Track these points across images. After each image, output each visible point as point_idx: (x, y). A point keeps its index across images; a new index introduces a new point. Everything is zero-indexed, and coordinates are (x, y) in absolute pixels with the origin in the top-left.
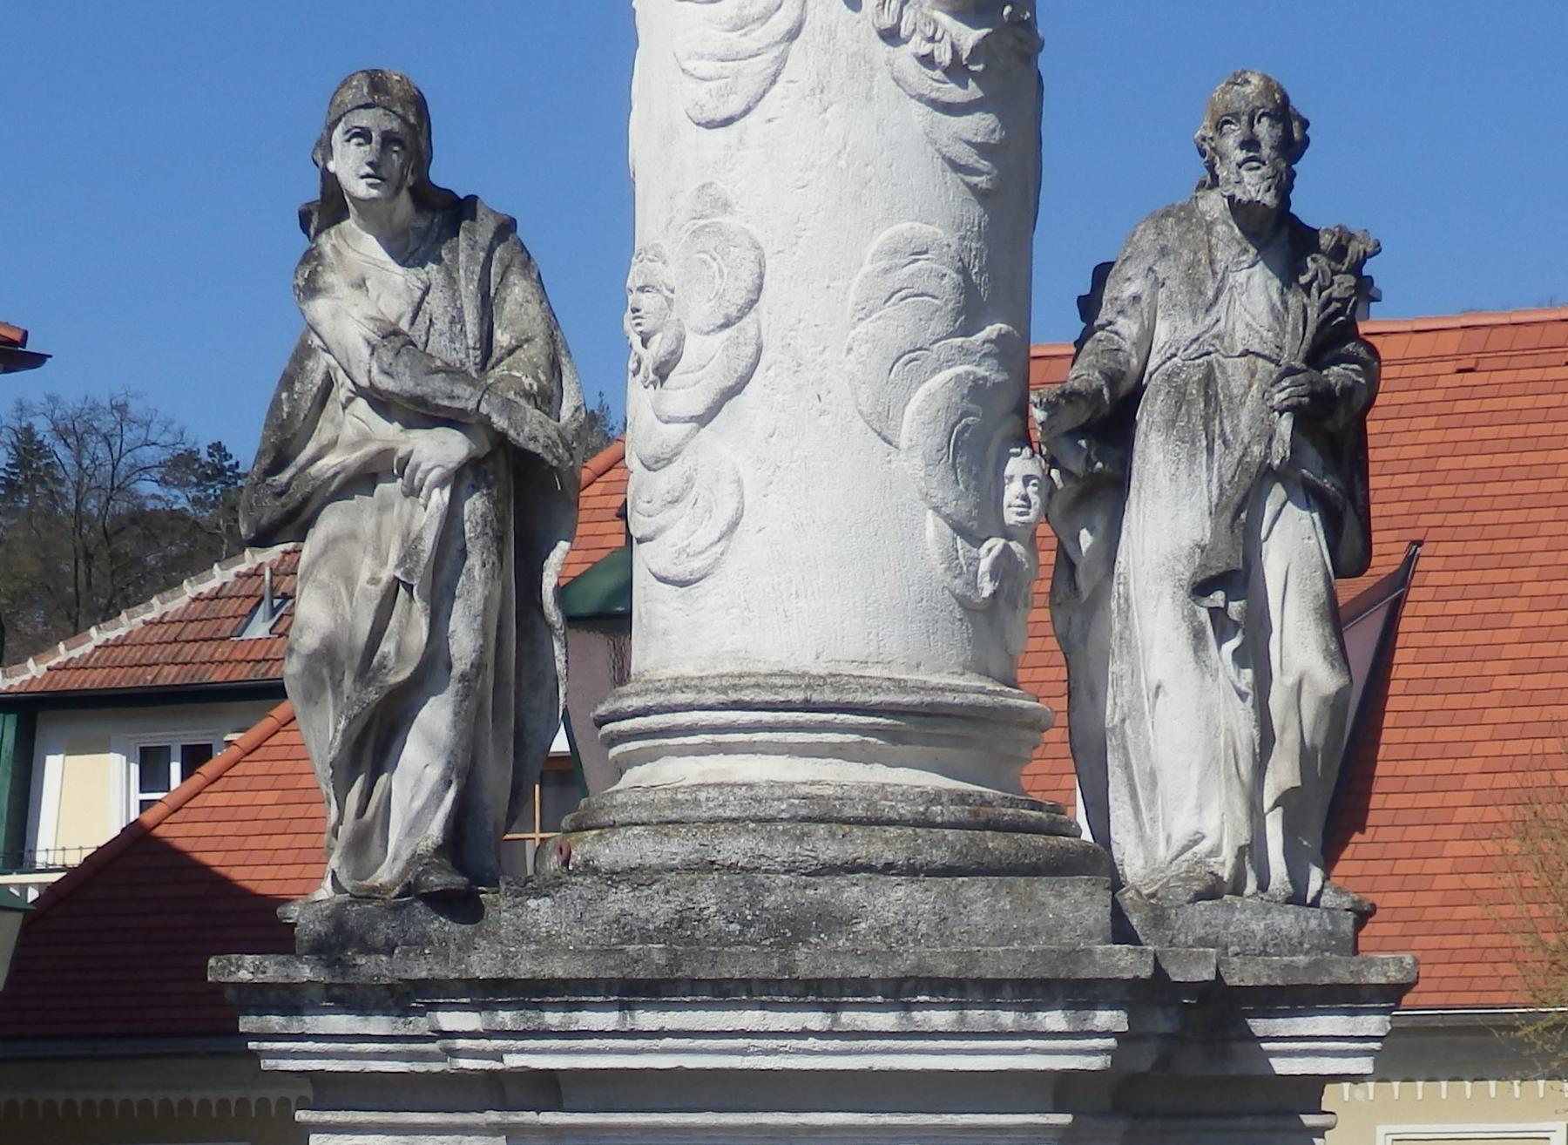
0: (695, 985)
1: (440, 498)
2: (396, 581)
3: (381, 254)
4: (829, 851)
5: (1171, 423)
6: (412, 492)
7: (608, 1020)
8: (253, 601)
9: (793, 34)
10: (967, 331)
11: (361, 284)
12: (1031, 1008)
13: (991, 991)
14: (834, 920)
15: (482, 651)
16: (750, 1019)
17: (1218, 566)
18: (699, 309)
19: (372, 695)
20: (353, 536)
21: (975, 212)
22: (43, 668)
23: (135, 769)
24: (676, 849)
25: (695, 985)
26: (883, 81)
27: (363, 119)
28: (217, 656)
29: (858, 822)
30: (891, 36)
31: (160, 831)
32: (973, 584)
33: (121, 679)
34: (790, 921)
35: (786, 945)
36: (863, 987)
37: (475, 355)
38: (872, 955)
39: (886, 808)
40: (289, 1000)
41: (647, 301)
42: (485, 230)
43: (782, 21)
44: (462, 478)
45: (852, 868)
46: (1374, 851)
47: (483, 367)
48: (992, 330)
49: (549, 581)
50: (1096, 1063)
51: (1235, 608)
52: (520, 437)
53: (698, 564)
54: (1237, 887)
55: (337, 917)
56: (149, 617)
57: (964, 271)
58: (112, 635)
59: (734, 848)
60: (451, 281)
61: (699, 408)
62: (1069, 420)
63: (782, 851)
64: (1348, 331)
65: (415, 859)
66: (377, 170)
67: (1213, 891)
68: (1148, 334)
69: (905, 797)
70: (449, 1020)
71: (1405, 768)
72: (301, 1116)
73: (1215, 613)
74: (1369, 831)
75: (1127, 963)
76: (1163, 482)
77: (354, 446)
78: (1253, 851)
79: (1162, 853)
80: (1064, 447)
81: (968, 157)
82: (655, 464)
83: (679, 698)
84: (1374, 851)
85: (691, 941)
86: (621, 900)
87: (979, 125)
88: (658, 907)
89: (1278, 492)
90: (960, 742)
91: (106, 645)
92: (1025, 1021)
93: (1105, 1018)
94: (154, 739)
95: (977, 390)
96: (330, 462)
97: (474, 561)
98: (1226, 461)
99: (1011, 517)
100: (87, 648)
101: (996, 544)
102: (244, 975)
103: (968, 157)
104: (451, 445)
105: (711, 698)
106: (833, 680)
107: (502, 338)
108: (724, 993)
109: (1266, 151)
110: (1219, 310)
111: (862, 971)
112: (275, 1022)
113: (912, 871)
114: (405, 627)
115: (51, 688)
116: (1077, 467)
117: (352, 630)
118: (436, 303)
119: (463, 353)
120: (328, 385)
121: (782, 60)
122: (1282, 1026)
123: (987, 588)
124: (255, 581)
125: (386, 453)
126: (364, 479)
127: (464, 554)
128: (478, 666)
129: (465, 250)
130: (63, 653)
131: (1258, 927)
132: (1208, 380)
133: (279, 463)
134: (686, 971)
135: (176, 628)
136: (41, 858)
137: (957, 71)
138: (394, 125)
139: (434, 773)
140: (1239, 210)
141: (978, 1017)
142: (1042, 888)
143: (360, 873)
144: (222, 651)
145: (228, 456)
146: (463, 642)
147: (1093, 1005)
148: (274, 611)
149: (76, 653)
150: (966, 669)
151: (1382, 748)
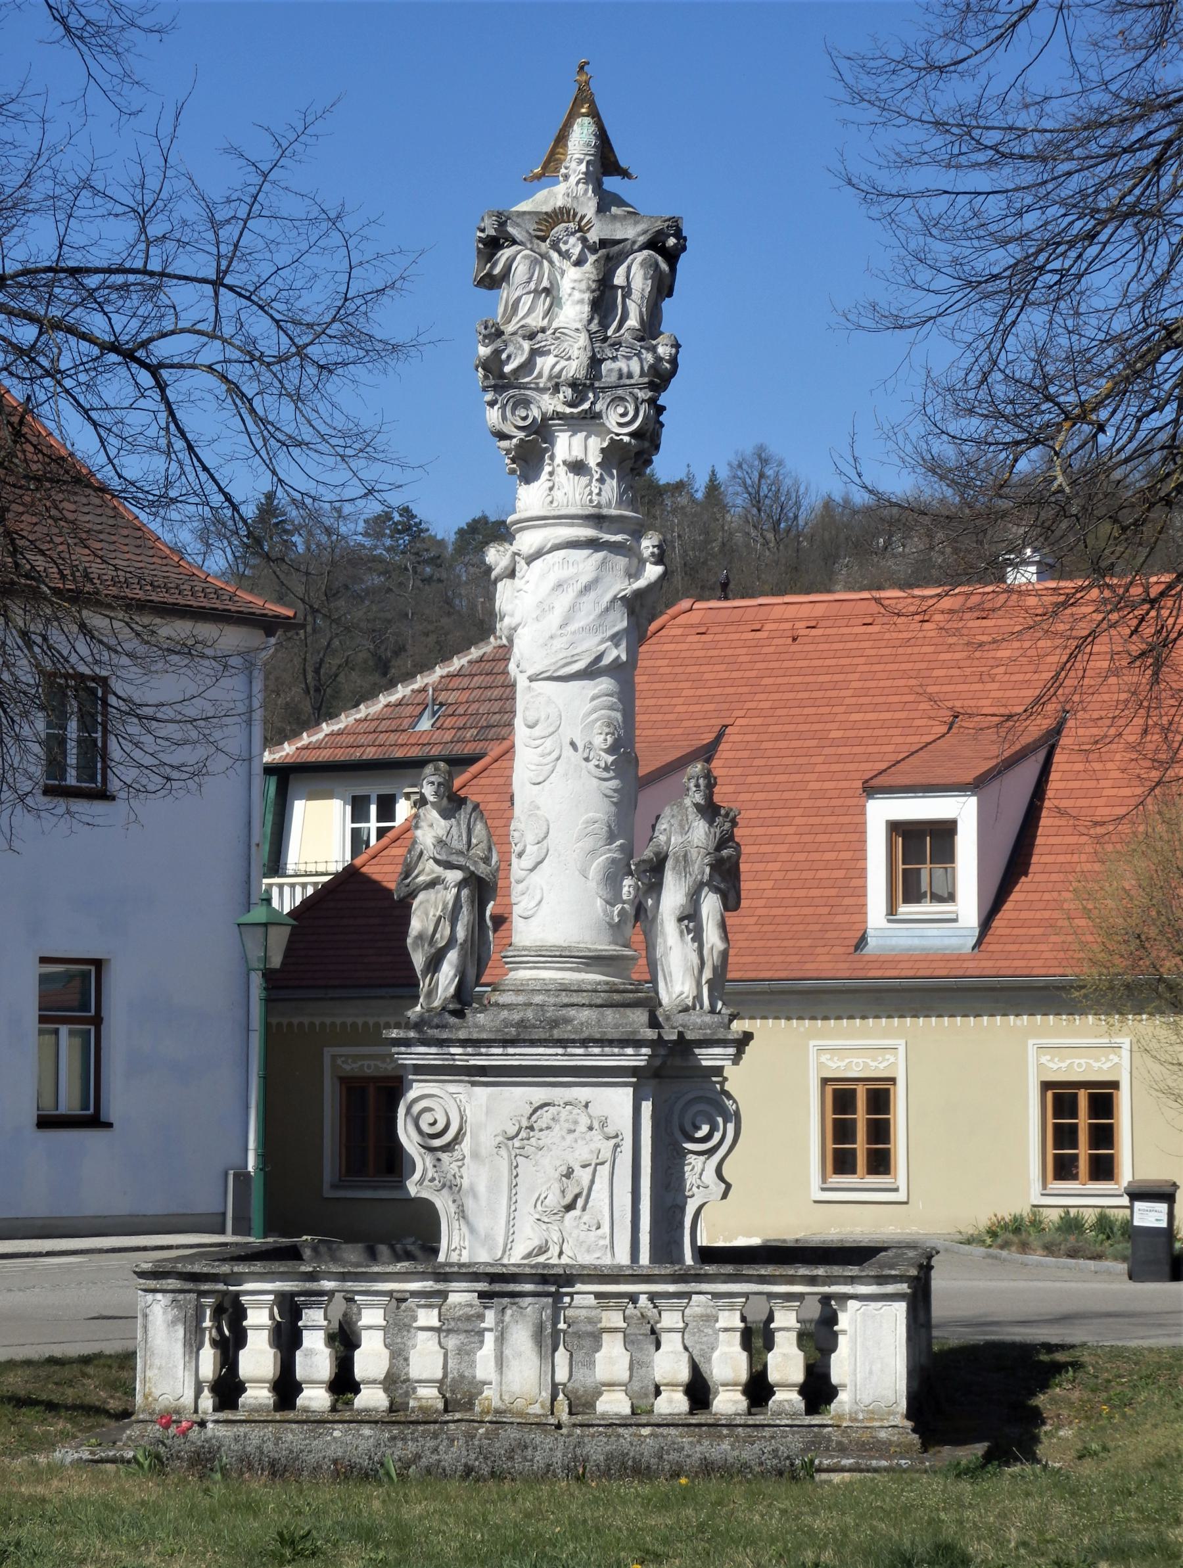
0: (524, 1041)
1: (455, 891)
2: (440, 917)
3: (437, 816)
4: (566, 1000)
5: (674, 869)
6: (446, 888)
7: (499, 1051)
8: (420, 708)
9: (558, 759)
10: (610, 844)
11: (431, 825)
12: (623, 1047)
13: (611, 1043)
14: (567, 1021)
15: (467, 936)
16: (541, 1050)
17: (686, 913)
18: (530, 838)
19: (433, 950)
20: (428, 901)
21: (613, 809)
22: (294, 748)
23: (349, 808)
24: (521, 999)
25: (524, 1041)
26: (584, 772)
27: (432, 779)
28: (400, 741)
29: (575, 991)
30: (587, 759)
31: (364, 870)
32: (612, 918)
33: (341, 755)
34: (554, 1021)
35: (552, 1028)
36: (573, 1041)
37: (466, 847)
38: (576, 1032)
39: (584, 987)
40: (407, 1043)
41: (516, 834)
42: (469, 807)
43: (555, 755)
44: (461, 885)
45: (573, 1005)
46: (1033, 887)
47: (468, 850)
48: (618, 843)
49: (488, 913)
50: (642, 1063)
51: (691, 925)
52: (478, 873)
53: (530, 913)
54: (694, 1008)
55: (421, 1016)
56: (358, 716)
57: (609, 826)
58: (336, 728)
59: (538, 999)
60: (459, 824)
61: (530, 867)
62: (642, 868)
63: (552, 1000)
64: (731, 837)
65: (445, 999)
66: (436, 793)
67: (686, 1009)
68: (669, 839)
69: (590, 983)
70: (453, 1050)
71: (1053, 840)
72: (411, 1077)
73: (687, 927)
74: (1030, 876)
75: (651, 1034)
76: (672, 886)
77: (428, 874)
78: (698, 997)
79: (674, 996)
80: (642, 876)
81: (611, 793)
82: (519, 882)
83: (524, 953)
84: (1033, 887)
85: (525, 1027)
86: (505, 1014)
87: (614, 784)
88: (516, 1016)
89: (706, 889)
90: (608, 966)
91: (332, 734)
92: (621, 1051)
93: (644, 1051)
94: (360, 791)
95: (613, 861)
96: (421, 879)
97: (464, 909)
98: (690, 880)
99: (625, 897)
100: (321, 736)
101: (619, 906)
102: (394, 1035)
103: (611, 793)
104: (454, 876)
105: (533, 953)
106: (569, 948)
107: (474, 841)
108: (533, 1043)
109: (702, 788)
110: (689, 834)
111: (573, 1037)
112: (403, 1049)
113: (590, 1006)
114: (443, 930)
115: (299, 760)
116: (646, 881)
117: (427, 929)
118: (454, 831)
119: (461, 845)
120: (421, 853)
121: (555, 766)
122: (704, 1051)
123: (617, 920)
124: (422, 696)
125: (438, 877)
126: (432, 884)
127: (461, 907)
128: (465, 941)
129: (463, 815)
130: (306, 739)
131: (699, 1021)
132: (685, 856)
133: (406, 877)
134: (522, 1037)
135: (375, 723)
136: (291, 868)
137: (606, 769)
138: (441, 780)
139: (452, 973)
140: (697, 805)
141: (607, 1050)
142: (628, 1011)
143: (429, 1004)
144: (403, 738)
145: (414, 517)
146: (461, 934)
147: (641, 1047)
148: (434, 713)
149: (314, 739)
150: (610, 943)
151: (1040, 829)
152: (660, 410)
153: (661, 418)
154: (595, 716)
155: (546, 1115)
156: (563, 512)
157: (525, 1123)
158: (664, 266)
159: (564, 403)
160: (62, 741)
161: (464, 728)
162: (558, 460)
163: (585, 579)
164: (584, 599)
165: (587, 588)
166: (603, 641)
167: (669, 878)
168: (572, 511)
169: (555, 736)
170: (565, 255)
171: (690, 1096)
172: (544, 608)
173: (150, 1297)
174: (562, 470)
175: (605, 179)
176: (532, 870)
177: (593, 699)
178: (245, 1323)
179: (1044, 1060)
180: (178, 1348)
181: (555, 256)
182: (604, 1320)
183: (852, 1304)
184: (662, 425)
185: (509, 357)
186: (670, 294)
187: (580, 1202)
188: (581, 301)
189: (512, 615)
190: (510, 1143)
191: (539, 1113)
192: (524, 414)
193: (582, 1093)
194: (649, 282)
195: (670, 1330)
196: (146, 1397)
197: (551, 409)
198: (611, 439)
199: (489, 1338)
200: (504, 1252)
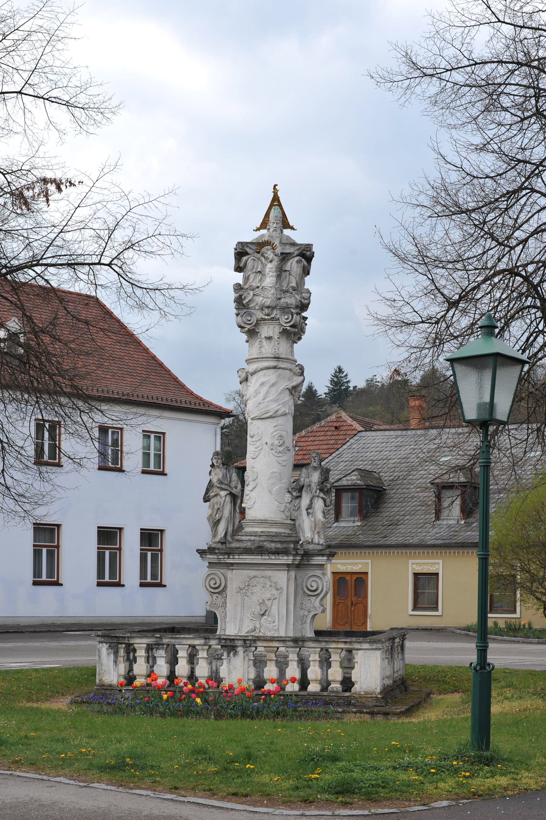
1: (224, 498)
9: (261, 449)
43: (260, 448)
59: (252, 538)
152: (305, 318)
153: (306, 322)
154: (275, 433)
155: (254, 581)
156: (264, 356)
157: (247, 584)
158: (306, 263)
159: (265, 315)
160: (149, 454)
161: (305, 455)
162: (263, 337)
163: (272, 382)
164: (272, 389)
165: (273, 385)
166: (279, 405)
167: (304, 494)
168: (268, 356)
169: (260, 441)
170: (266, 259)
171: (312, 574)
172: (257, 393)
173: (101, 645)
174: (264, 341)
175: (284, 230)
176: (251, 491)
177: (275, 427)
178: (178, 656)
179: (414, 566)
180: (112, 663)
181: (263, 259)
182: (268, 656)
183: (360, 652)
184: (306, 324)
185: (245, 297)
186: (308, 274)
187: (267, 613)
188: (272, 276)
189: (246, 396)
190: (241, 591)
191: (252, 580)
192: (249, 319)
193: (268, 573)
194: (299, 269)
195: (292, 660)
196: (100, 681)
197: (260, 317)
198: (283, 329)
199: (225, 661)
200: (239, 631)
